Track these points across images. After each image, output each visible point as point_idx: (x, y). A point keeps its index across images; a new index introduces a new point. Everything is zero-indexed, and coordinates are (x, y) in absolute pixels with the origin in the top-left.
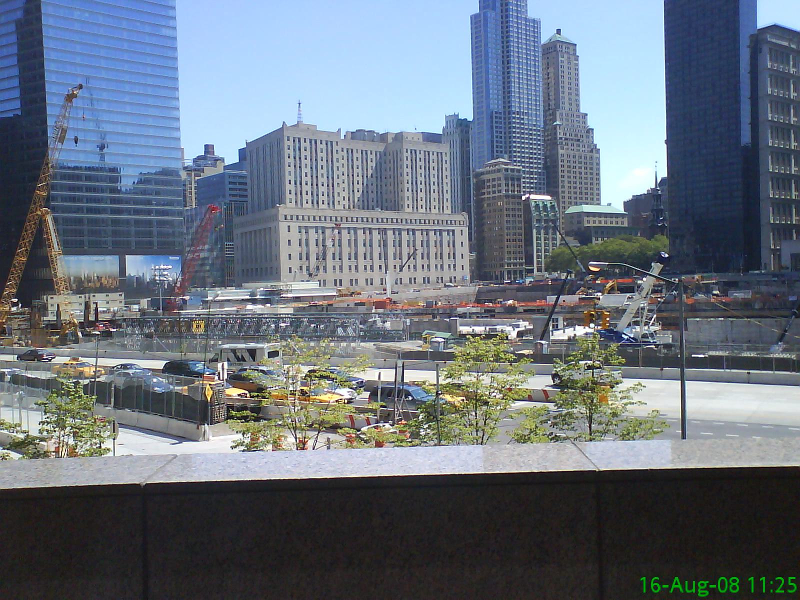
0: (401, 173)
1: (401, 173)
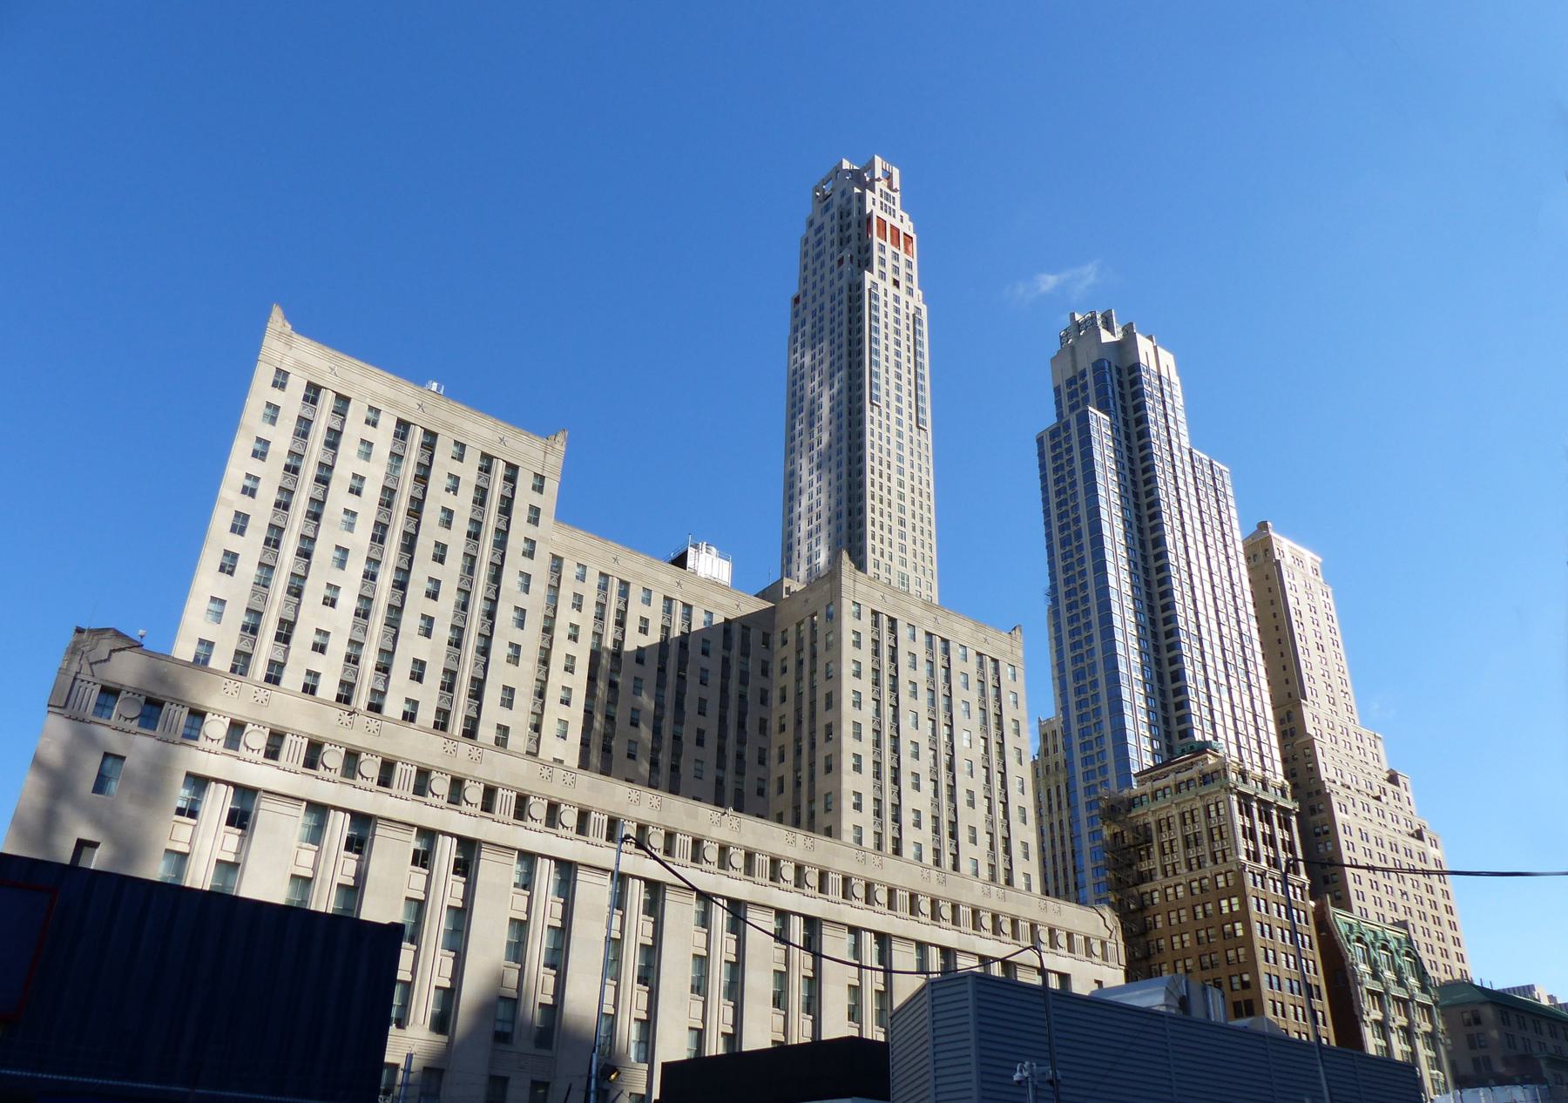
0: (829, 696)
1: (829, 696)
